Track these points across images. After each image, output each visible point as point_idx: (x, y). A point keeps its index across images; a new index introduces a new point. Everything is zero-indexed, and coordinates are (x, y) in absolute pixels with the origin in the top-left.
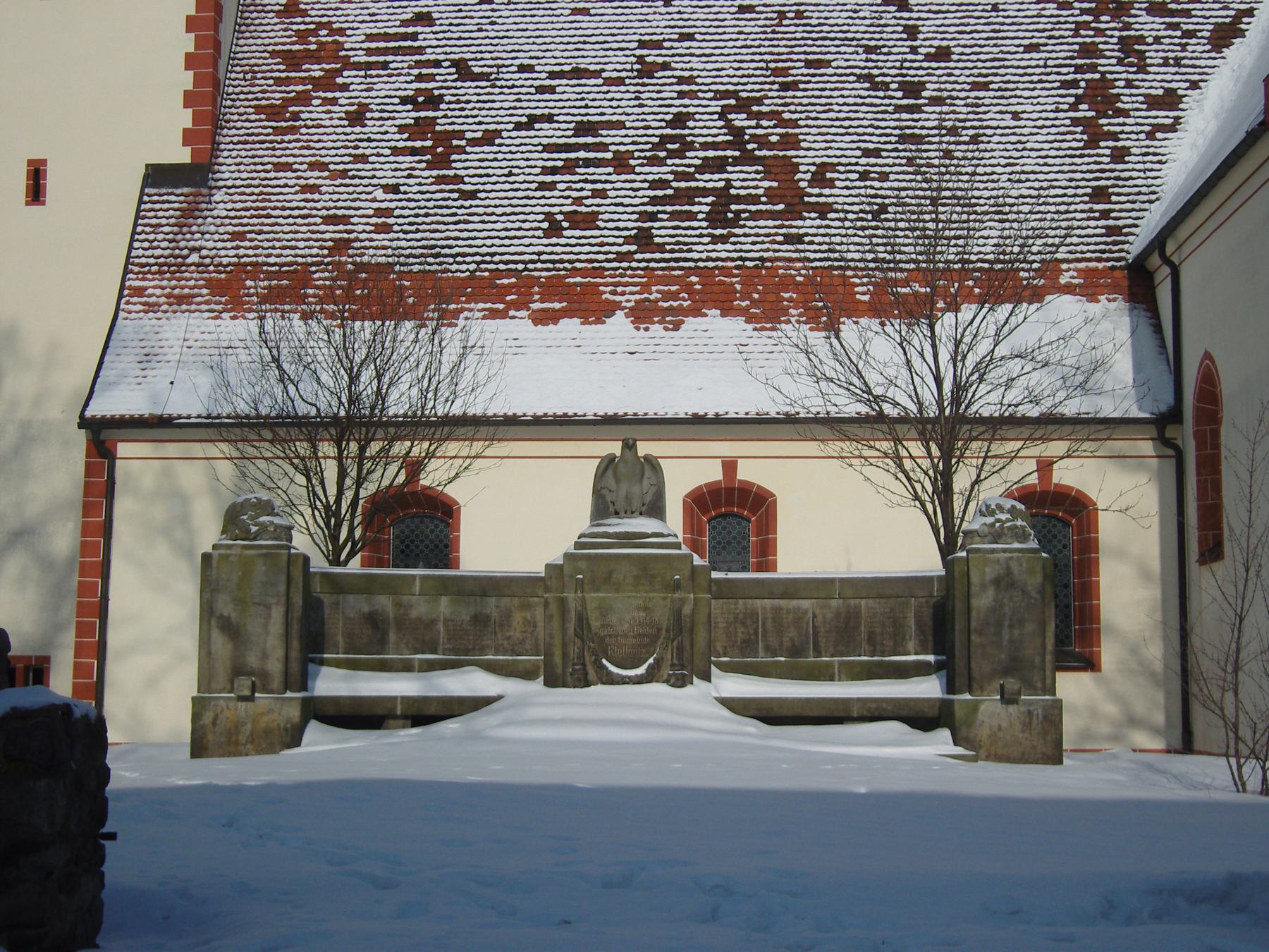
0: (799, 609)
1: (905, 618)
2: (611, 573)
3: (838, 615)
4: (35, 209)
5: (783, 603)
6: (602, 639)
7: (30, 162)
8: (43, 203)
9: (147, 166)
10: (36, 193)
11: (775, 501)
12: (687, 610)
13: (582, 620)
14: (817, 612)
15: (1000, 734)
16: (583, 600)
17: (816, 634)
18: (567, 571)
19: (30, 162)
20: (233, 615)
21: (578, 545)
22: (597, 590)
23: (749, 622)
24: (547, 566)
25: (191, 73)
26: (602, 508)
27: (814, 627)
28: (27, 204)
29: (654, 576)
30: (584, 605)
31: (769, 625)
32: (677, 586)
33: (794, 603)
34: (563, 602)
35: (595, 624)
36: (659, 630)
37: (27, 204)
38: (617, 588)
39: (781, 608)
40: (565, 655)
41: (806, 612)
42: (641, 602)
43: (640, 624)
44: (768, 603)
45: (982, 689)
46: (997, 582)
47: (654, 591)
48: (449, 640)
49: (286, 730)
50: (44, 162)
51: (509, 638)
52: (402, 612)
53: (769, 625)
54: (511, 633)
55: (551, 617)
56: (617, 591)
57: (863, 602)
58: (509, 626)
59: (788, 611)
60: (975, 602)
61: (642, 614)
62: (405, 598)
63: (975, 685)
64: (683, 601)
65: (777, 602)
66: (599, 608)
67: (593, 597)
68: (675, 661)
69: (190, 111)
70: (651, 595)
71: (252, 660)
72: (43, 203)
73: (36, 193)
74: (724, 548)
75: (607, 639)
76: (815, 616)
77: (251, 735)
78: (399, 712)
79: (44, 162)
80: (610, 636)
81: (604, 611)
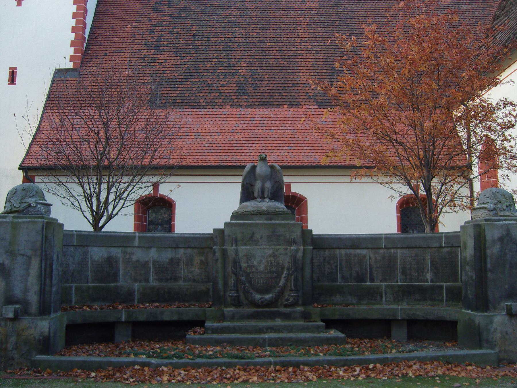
0: (360, 254)
1: (424, 259)
2: (253, 234)
3: (384, 258)
4: (12, 86)
5: (352, 251)
6: (248, 274)
7: (10, 68)
8: (15, 84)
9: (56, 69)
10: (12, 80)
11: (307, 201)
12: (300, 255)
13: (236, 263)
14: (371, 256)
15: (507, 337)
16: (236, 251)
17: (371, 269)
18: (226, 233)
19: (10, 68)
20: (7, 262)
21: (233, 217)
22: (245, 245)
23: (332, 262)
24: (214, 230)
25: (74, 34)
26: (242, 200)
27: (370, 265)
28: (9, 84)
29: (279, 236)
30: (237, 254)
31: (344, 264)
32: (293, 242)
33: (358, 251)
34: (224, 252)
35: (244, 265)
36: (283, 269)
37: (9, 84)
38: (256, 243)
39: (351, 254)
40: (226, 284)
41: (365, 257)
42: (271, 251)
43: (271, 265)
44: (343, 252)
45: (495, 308)
46: (501, 239)
47: (279, 245)
48: (156, 273)
49: (39, 340)
50: (16, 68)
51: (192, 272)
52: (127, 257)
53: (344, 264)
54: (193, 269)
55: (217, 260)
56: (256, 245)
57: (399, 251)
58: (192, 265)
59: (355, 255)
60: (489, 252)
61: (272, 259)
62: (129, 250)
63: (490, 306)
64: (297, 251)
65: (348, 251)
66: (247, 255)
67: (243, 249)
68: (293, 288)
69: (73, 48)
70: (278, 247)
71: (18, 292)
72: (15, 84)
73: (12, 80)
74: (408, 217)
75: (251, 275)
76: (370, 258)
77: (16, 343)
78: (123, 320)
79: (16, 68)
80: (253, 272)
81: (249, 257)
